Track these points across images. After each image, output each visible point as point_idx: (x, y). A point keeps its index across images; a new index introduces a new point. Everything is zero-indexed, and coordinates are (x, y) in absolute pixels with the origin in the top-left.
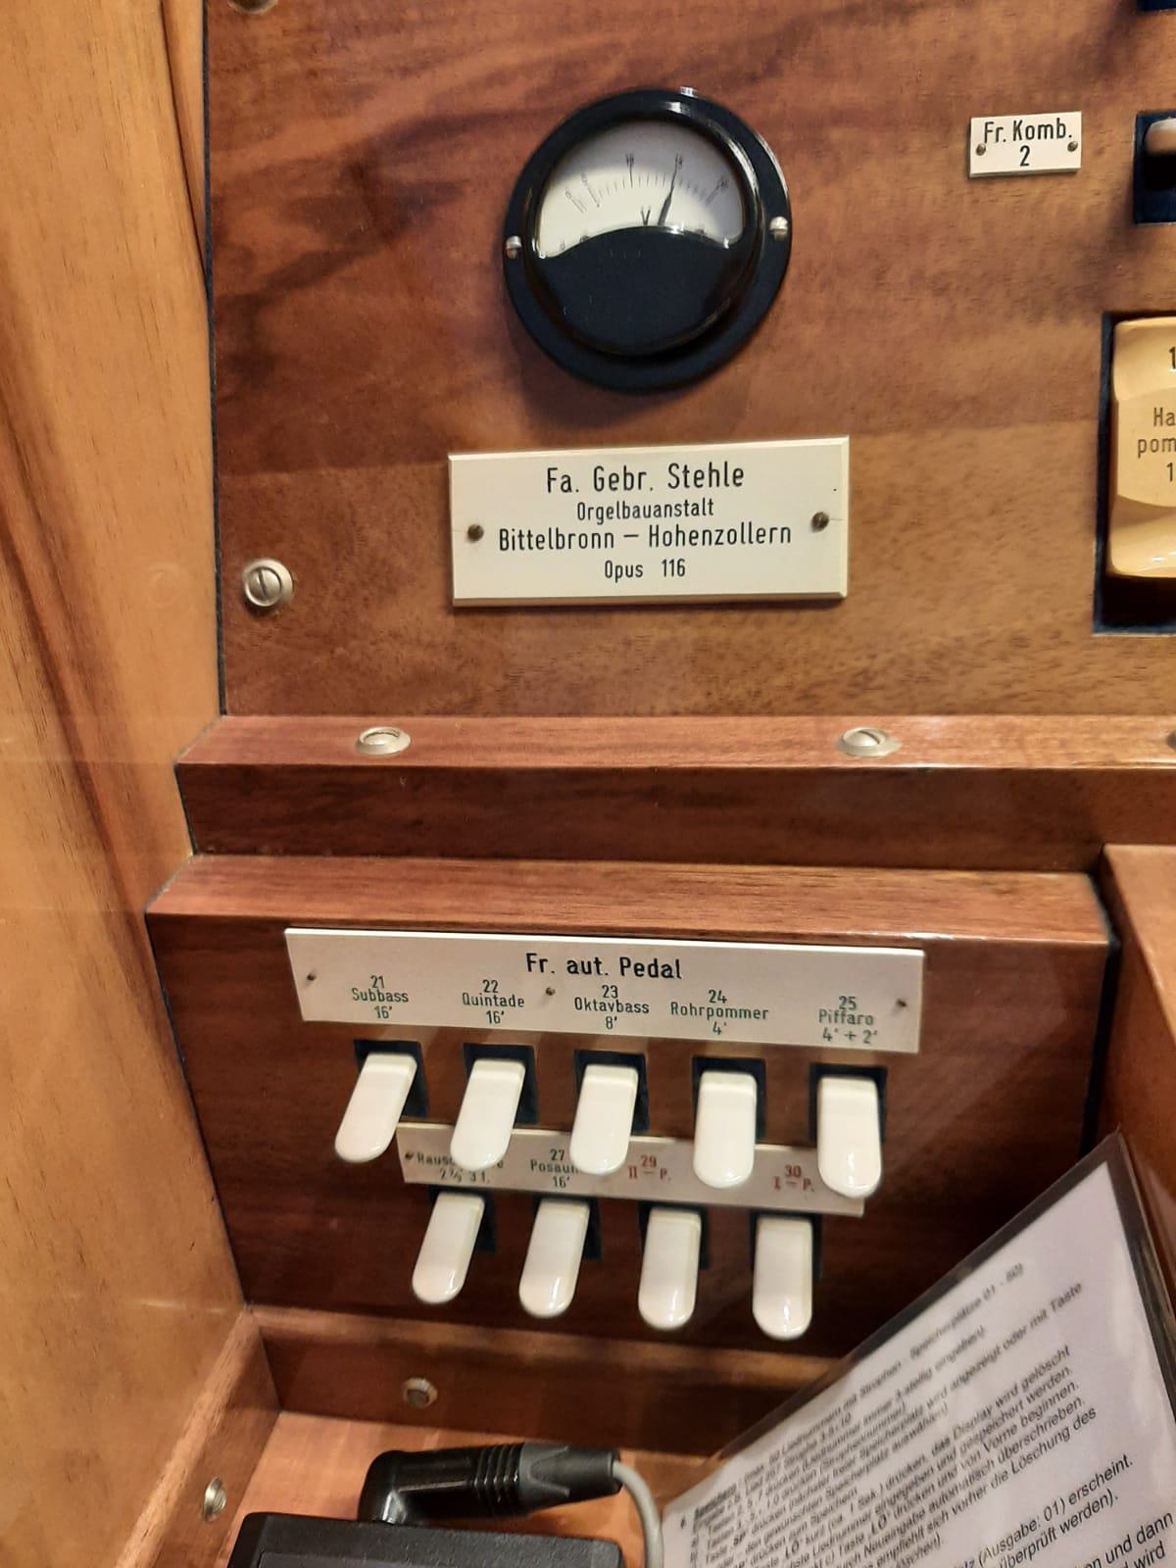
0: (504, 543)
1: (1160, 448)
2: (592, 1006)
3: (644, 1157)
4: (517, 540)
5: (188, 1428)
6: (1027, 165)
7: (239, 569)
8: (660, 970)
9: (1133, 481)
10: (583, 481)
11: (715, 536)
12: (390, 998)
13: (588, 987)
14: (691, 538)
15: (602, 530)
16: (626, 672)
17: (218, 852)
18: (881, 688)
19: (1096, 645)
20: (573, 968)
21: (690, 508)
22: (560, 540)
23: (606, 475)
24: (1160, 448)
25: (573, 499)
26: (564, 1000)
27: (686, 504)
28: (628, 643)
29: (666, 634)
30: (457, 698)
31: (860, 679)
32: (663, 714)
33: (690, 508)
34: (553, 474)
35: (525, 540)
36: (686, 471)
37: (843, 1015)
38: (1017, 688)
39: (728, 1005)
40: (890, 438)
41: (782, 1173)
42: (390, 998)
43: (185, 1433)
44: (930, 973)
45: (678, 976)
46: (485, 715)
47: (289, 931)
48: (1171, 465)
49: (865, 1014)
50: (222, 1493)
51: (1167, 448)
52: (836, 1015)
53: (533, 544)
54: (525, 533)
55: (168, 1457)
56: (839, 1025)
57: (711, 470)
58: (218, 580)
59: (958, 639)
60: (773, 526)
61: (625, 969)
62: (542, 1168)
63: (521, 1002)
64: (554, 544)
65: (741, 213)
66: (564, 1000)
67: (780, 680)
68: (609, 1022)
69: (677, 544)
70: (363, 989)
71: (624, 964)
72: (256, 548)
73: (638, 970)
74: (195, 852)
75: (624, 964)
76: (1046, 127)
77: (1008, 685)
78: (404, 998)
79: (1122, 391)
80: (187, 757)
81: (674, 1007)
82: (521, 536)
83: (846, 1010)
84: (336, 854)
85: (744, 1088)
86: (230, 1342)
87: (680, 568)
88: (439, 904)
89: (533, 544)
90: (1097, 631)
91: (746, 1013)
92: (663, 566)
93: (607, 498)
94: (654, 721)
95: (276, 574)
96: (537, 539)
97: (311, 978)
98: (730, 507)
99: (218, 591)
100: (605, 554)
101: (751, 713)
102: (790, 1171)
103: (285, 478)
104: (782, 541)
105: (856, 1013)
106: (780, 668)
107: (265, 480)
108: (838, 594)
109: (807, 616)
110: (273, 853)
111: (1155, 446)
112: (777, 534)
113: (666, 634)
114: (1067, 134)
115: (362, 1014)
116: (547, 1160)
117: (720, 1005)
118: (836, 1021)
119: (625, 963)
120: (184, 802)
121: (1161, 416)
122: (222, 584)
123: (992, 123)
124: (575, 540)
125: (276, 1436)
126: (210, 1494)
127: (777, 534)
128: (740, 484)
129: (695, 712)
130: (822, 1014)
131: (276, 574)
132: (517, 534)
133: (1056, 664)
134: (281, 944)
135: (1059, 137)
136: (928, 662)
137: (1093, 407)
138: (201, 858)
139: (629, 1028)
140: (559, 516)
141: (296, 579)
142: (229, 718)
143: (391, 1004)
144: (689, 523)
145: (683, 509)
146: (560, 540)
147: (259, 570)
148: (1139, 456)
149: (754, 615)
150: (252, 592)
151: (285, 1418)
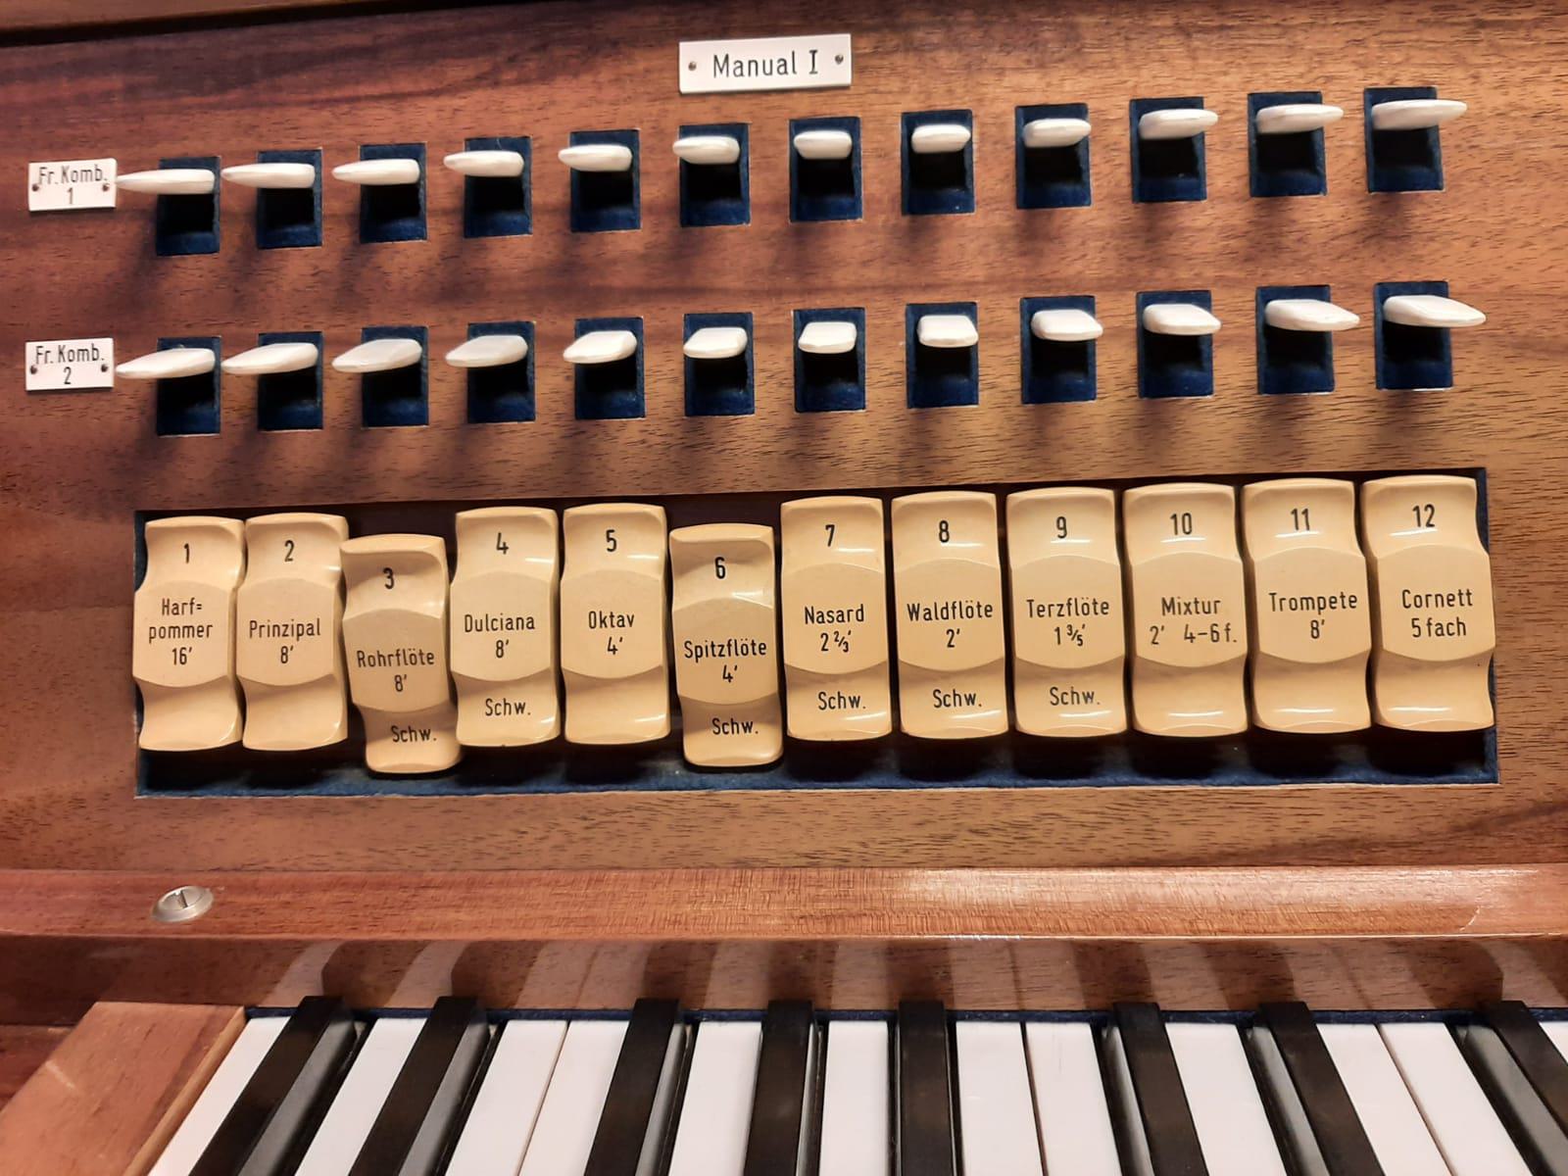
2: (1192, 607)
6: (69, 383)
11: (282, 629)
14: (1449, 600)
21: (615, 620)
27: (612, 616)
33: (615, 620)
54: (1464, 592)
69: (1302, 608)
76: (188, 627)
89: (1099, 610)
96: (1102, 605)
104: (1437, 605)
112: (1432, 600)
114: (101, 357)
121: (167, 606)
123: (41, 347)
124: (1286, 603)
127: (1432, 600)
135: (94, 359)
148: (150, 642)
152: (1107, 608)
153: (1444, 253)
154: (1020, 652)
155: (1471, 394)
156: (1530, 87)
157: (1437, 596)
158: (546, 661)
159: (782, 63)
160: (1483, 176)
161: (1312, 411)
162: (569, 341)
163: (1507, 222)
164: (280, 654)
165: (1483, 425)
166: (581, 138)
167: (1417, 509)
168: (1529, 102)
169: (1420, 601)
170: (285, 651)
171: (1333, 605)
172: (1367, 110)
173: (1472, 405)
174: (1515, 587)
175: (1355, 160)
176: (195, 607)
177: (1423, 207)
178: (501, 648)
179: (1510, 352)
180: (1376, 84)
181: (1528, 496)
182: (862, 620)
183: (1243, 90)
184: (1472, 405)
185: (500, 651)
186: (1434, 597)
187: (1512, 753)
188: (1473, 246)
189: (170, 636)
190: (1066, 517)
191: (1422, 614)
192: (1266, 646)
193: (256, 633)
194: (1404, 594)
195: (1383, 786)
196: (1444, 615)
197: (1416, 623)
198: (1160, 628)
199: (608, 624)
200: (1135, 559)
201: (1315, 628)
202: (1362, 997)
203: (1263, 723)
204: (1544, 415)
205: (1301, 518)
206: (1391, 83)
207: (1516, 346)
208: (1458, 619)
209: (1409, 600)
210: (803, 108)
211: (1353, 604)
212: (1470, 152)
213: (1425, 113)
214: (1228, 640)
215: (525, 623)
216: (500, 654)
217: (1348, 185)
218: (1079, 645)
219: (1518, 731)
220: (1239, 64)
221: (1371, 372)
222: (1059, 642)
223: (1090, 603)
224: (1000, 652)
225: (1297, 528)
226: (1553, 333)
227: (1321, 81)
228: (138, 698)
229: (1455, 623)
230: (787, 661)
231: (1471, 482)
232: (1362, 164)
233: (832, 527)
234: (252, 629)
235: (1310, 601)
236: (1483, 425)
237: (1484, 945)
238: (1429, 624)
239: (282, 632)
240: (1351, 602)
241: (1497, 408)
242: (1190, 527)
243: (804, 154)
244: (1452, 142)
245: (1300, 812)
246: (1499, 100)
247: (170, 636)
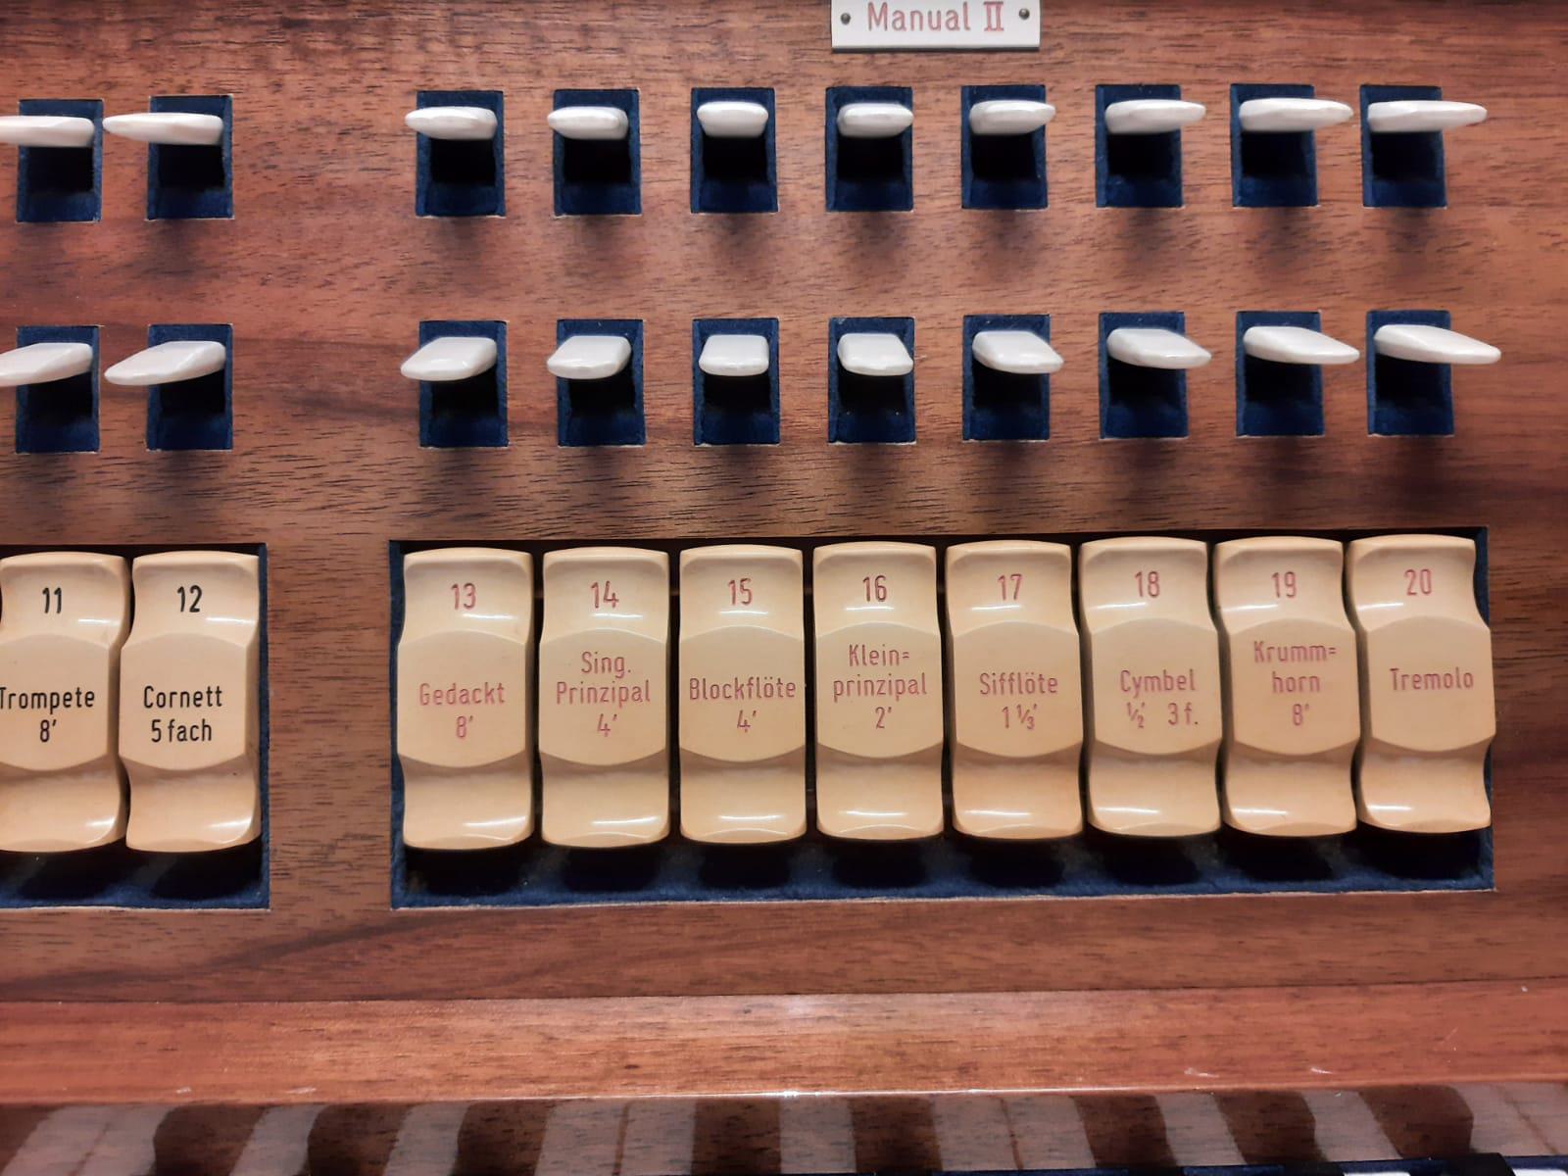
0: (695, 691)
1: (721, 689)
2: (745, 690)
11: (600, 693)
14: (196, 699)
24: (721, 689)
35: (1007, 685)
48: (1019, 706)
51: (1149, 687)
53: (783, 693)
54: (213, 689)
61: (562, 696)
65: (249, 691)
76: (39, 695)
89: (783, 693)
112: (176, 699)
124: (15, 700)
127: (176, 699)
128: (90, 706)
148: (836, 700)
152: (92, 699)
153: (230, 292)
154: (823, 738)
155: (252, 458)
156: (339, 99)
158: (518, 744)
159: (898, 16)
160: (279, 203)
161: (73, 475)
162: (409, 351)
163: (304, 257)
164: (1291, 714)
165: (264, 494)
166: (566, 98)
167: (181, 590)
168: (335, 115)
169: (163, 700)
170: (45, 726)
171: (68, 703)
172: (965, 110)
173: (254, 470)
174: (296, 682)
175: (134, 180)
177: (209, 236)
178: (46, 730)
179: (299, 410)
180: (164, 92)
181: (315, 577)
183: (14, 96)
184: (254, 470)
185: (45, 734)
187: (287, 874)
188: (263, 284)
190: (202, 588)
191: (164, 715)
192: (962, 737)
193: (565, 697)
194: (1122, 677)
195: (144, 910)
196: (188, 717)
197: (157, 725)
199: (746, 694)
200: (956, 630)
201: (45, 729)
202: (1547, 1144)
203: (1371, 819)
204: (334, 484)
205: (54, 598)
206: (183, 91)
207: (305, 402)
208: (204, 721)
209: (152, 698)
210: (860, 75)
211: (1053, 689)
212: (266, 173)
213: (1005, 118)
214: (1188, 721)
215: (630, 695)
216: (45, 737)
217: (125, 211)
218: (1029, 728)
219: (292, 849)
220: (11, 65)
221: (141, 430)
222: (1007, 726)
223: (774, 682)
224: (800, 740)
225: (1004, 598)
226: (351, 388)
227: (102, 87)
228: (397, 775)
229: (200, 725)
230: (683, 743)
231: (1468, 543)
232: (143, 184)
233: (1019, 575)
234: (559, 692)
235: (1156, 681)
236: (264, 494)
237: (1452, 1086)
238: (171, 727)
239: (876, 690)
240: (1050, 685)
241: (281, 474)
242: (1430, 586)
243: (709, 130)
244: (245, 160)
245: (49, 939)
246: (302, 112)
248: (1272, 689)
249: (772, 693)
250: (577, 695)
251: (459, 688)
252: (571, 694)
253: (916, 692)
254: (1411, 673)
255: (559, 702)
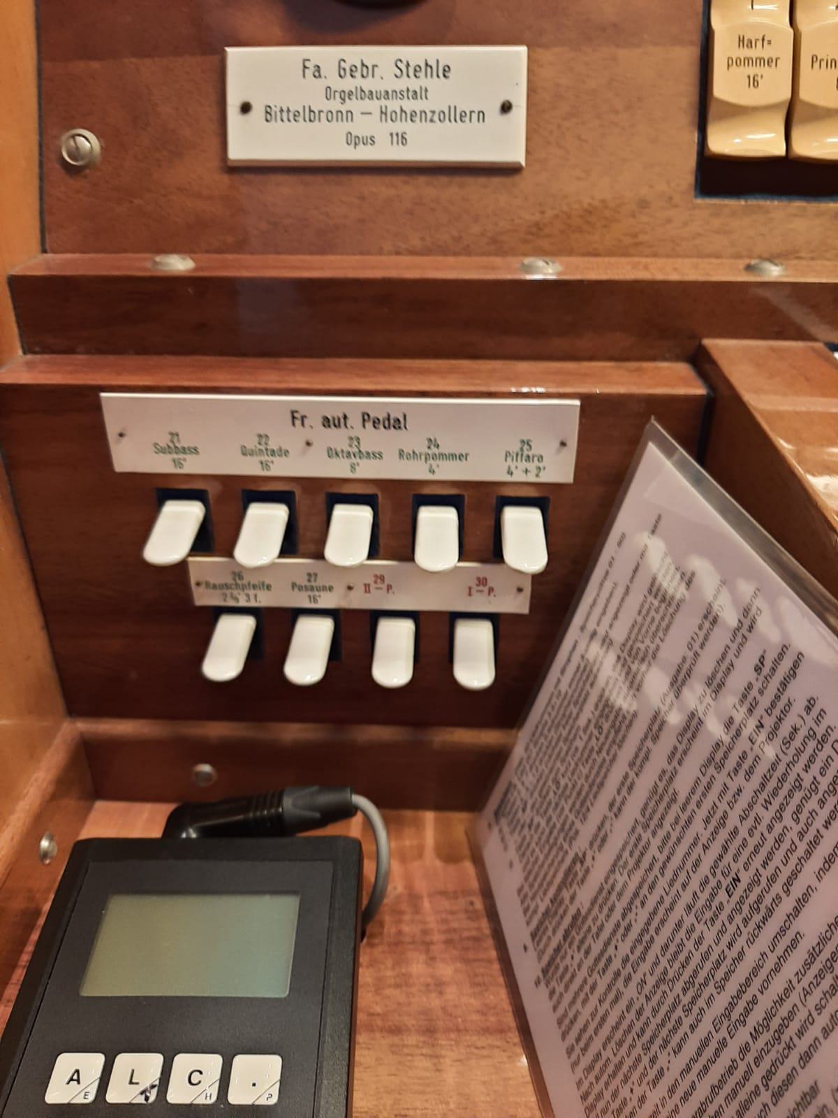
3: (376, 576)
4: (279, 114)
5: (27, 793)
7: (57, 137)
8: (392, 422)
9: (725, 86)
10: (330, 70)
11: (429, 115)
12: (184, 450)
13: (337, 437)
15: (344, 109)
16: (362, 221)
17: (43, 352)
18: (549, 236)
19: (695, 207)
20: (327, 422)
22: (312, 115)
23: (347, 66)
25: (321, 84)
26: (319, 451)
27: (408, 90)
28: (363, 198)
29: (392, 192)
30: (230, 239)
31: (534, 230)
32: (390, 253)
34: (307, 64)
35: (285, 115)
36: (408, 65)
37: (522, 455)
38: (642, 238)
39: (443, 450)
40: (557, 50)
41: (473, 583)
42: (184, 450)
43: (24, 797)
44: (584, 421)
45: (406, 428)
46: (252, 253)
47: (103, 395)
49: (537, 453)
50: (54, 844)
52: (517, 455)
54: (285, 109)
55: (12, 812)
56: (519, 463)
57: (427, 64)
58: (40, 146)
59: (603, 201)
60: (472, 110)
62: (300, 588)
63: (287, 452)
64: (307, 119)
66: (319, 451)
67: (476, 229)
68: (353, 468)
70: (163, 444)
71: (365, 417)
72: (71, 122)
73: (376, 423)
74: (25, 353)
75: (365, 417)
77: (635, 236)
78: (195, 451)
79: (718, 22)
80: (17, 270)
81: (401, 453)
82: (282, 110)
83: (525, 451)
84: (138, 353)
85: (449, 515)
86: (58, 740)
87: (403, 139)
88: (222, 380)
89: (411, 73)
90: (696, 197)
91: (453, 456)
92: (390, 138)
93: (348, 84)
94: (383, 258)
95: (88, 142)
97: (121, 435)
98: (440, 94)
99: (41, 154)
100: (346, 126)
101: (455, 254)
102: (479, 582)
103: (95, 65)
105: (530, 453)
106: (476, 219)
107: (79, 66)
108: (519, 163)
109: (496, 181)
110: (88, 352)
111: (740, 62)
112: (475, 116)
113: (392, 192)
115: (162, 465)
116: (304, 582)
117: (434, 450)
118: (517, 460)
119: (366, 417)
120: (15, 308)
122: (44, 149)
125: (93, 816)
126: (45, 844)
127: (475, 116)
129: (413, 252)
130: (507, 454)
131: (88, 142)
132: (278, 110)
133: (669, 221)
134: (97, 407)
136: (581, 217)
137: (697, 37)
138: (29, 357)
139: (368, 470)
140: (311, 94)
141: (104, 145)
142: (49, 256)
143: (185, 456)
144: (409, 105)
145: (405, 94)
146: (312, 115)
147: (73, 137)
149: (458, 179)
150: (69, 157)
151: (100, 805)
157: (479, 112)
176: (765, 43)
182: (728, 58)
186: (477, 113)
189: (337, 120)
193: (816, 65)
198: (816, 698)
234: (364, 420)
239: (429, 118)
247: (337, 120)
248: (637, 612)
249: (740, 64)
250: (824, 64)
251: (392, 417)
252: (820, 62)
253: (400, 428)
254: (339, 90)
255: (304, 76)
